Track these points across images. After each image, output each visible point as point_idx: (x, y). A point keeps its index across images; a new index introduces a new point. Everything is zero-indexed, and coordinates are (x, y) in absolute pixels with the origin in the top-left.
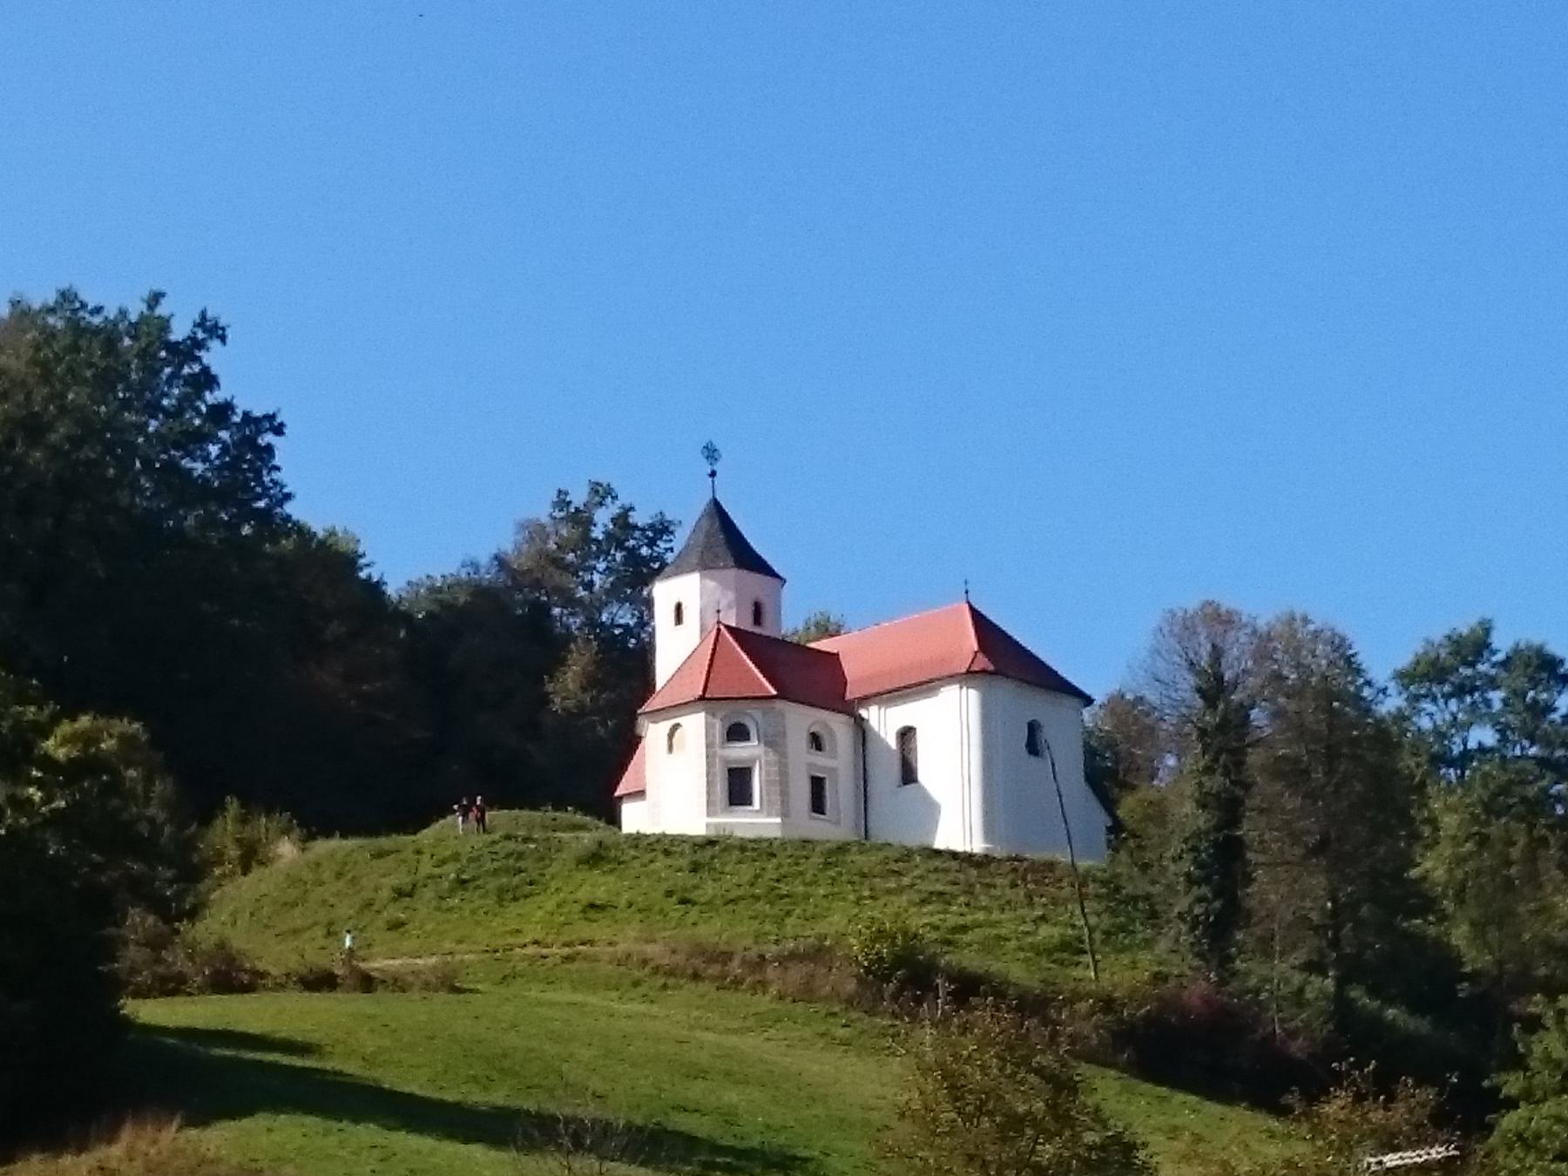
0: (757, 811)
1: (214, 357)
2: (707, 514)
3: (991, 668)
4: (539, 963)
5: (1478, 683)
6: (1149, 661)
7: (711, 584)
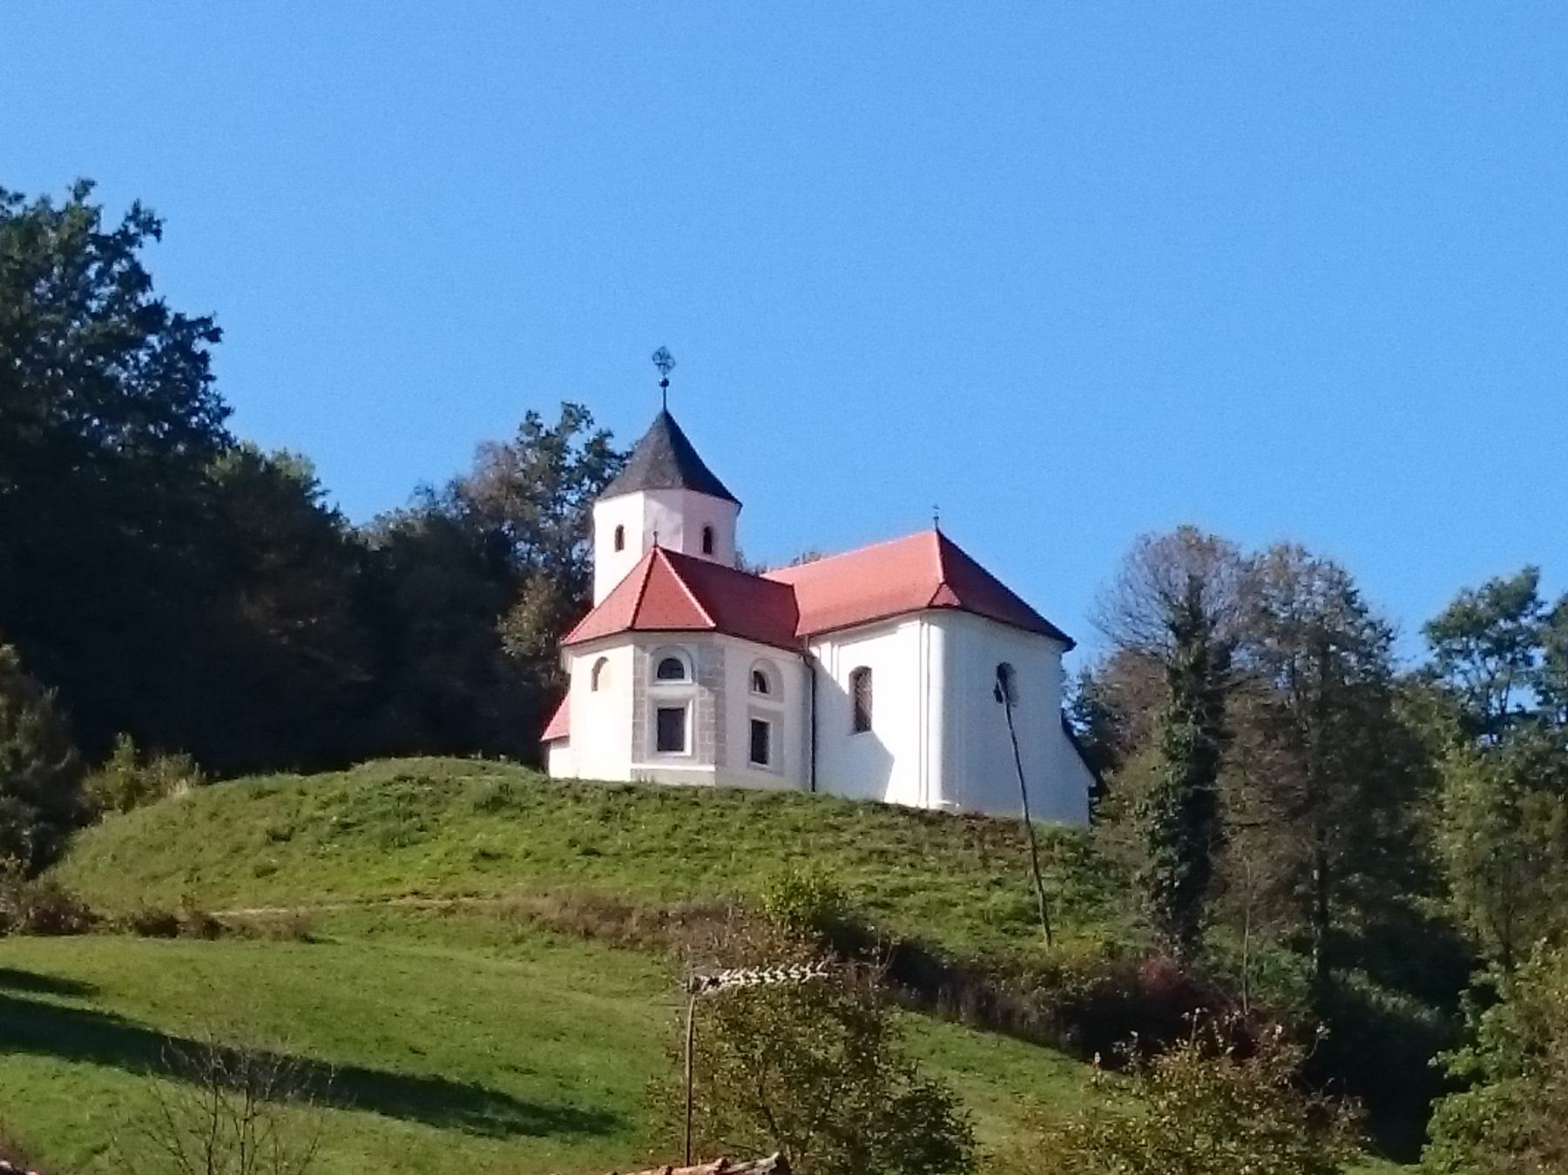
0: (689, 758)
1: (147, 254)
2: (655, 427)
3: (956, 602)
4: (413, 915)
5: (1519, 638)
6: (1117, 592)
7: (656, 506)
